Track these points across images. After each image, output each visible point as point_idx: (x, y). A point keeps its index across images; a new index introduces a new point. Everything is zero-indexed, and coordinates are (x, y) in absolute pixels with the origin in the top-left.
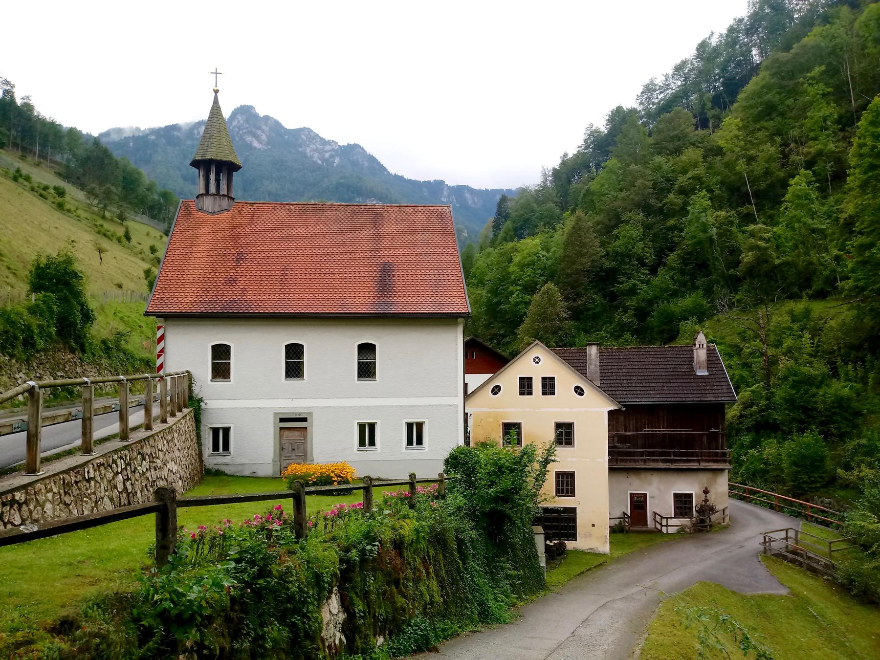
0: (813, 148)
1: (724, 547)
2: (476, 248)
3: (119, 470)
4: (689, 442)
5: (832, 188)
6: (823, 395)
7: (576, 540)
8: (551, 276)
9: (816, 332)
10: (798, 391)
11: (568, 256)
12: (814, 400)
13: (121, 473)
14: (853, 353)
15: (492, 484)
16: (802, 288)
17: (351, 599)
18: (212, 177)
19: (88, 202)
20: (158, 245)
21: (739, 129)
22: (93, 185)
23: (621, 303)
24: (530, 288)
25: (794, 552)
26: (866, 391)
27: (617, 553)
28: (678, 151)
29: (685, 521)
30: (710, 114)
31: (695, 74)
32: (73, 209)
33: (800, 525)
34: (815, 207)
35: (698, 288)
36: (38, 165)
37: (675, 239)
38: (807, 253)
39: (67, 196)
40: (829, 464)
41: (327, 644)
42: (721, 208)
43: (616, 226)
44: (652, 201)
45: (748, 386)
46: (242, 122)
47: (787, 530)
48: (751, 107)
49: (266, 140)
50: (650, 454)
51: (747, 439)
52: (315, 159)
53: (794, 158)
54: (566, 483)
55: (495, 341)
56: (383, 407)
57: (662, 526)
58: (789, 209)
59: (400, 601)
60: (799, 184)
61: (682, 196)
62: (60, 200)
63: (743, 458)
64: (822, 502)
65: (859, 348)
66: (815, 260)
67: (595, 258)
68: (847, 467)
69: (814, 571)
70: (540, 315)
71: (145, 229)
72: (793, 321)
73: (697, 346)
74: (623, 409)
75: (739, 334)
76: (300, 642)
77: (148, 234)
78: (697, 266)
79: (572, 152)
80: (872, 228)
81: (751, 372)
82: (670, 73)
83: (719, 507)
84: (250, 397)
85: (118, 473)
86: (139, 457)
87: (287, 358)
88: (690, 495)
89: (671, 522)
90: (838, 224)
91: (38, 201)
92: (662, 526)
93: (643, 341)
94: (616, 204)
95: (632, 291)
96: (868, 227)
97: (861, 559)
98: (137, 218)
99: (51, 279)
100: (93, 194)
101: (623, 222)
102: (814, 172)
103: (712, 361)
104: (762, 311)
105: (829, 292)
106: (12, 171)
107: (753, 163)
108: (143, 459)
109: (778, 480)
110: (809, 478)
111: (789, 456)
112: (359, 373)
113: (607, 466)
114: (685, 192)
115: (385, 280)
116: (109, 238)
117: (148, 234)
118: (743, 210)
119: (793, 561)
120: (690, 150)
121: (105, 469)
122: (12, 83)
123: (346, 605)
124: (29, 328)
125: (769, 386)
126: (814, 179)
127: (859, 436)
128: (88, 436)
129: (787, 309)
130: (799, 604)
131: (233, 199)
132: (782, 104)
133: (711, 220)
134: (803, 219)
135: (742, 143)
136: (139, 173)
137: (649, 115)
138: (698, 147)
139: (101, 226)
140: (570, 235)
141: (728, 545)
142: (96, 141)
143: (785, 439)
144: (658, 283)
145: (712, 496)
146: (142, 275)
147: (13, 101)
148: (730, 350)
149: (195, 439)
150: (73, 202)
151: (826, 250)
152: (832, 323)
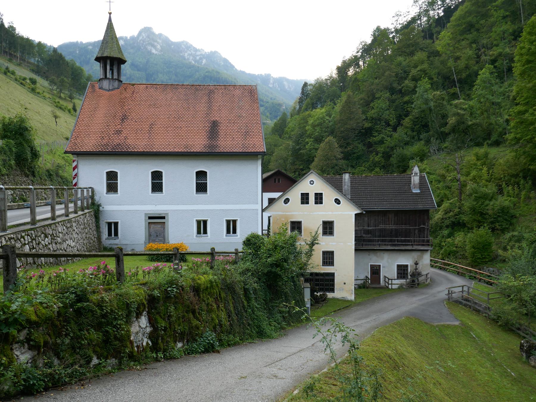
0: (495, 52)
1: (424, 297)
2: (289, 115)
3: (27, 242)
4: (407, 233)
5: (507, 77)
6: (492, 205)
7: (334, 292)
8: (332, 133)
9: (491, 166)
10: (478, 203)
11: (343, 120)
12: (487, 208)
13: (28, 244)
14: (513, 180)
15: (270, 256)
16: (485, 139)
17: (156, 319)
18: (108, 67)
19: (50, 87)
21: (451, 39)
22: (54, 77)
24: (319, 140)
25: (467, 300)
26: (519, 203)
27: (359, 300)
28: (412, 54)
29: (403, 281)
30: (434, 31)
31: (426, 5)
32: (41, 92)
33: (473, 284)
34: (495, 88)
35: (421, 140)
36: (19, 65)
37: (409, 109)
38: (488, 118)
39: (37, 84)
40: (494, 247)
41: (135, 345)
42: (437, 89)
43: (372, 101)
44: (395, 85)
45: (448, 200)
46: (145, 37)
47: (463, 287)
48: (458, 25)
50: (383, 241)
51: (446, 232)
52: (190, 61)
53: (483, 58)
54: (328, 258)
55: (297, 173)
58: (478, 90)
59: (195, 322)
60: (485, 73)
61: (414, 82)
63: (443, 244)
64: (489, 270)
65: (516, 176)
66: (493, 122)
67: (359, 121)
68: (505, 249)
69: (478, 311)
70: (324, 157)
72: (478, 160)
73: (414, 174)
74: (364, 212)
75: (445, 168)
76: (110, 342)
78: (422, 126)
80: (527, 100)
81: (450, 191)
83: (424, 273)
84: (130, 204)
85: (25, 244)
86: (42, 235)
87: (152, 180)
88: (407, 266)
89: (394, 282)
90: (509, 100)
91: (19, 87)
93: (387, 172)
94: (373, 87)
95: (381, 142)
96: (524, 100)
97: (505, 304)
100: (54, 83)
101: (376, 98)
102: (495, 67)
103: (422, 184)
106: (3, 69)
107: (458, 61)
108: (46, 236)
109: (464, 257)
110: (482, 255)
111: (470, 242)
114: (415, 79)
115: (214, 129)
116: (63, 110)
118: (452, 91)
119: (465, 305)
120: (419, 53)
121: (15, 241)
123: (152, 322)
125: (461, 200)
126: (494, 70)
127: (513, 231)
128: (4, 221)
129: (474, 152)
130: (465, 330)
131: (122, 81)
132: (478, 23)
133: (431, 97)
134: (486, 96)
135: (451, 48)
136: (82, 70)
138: (424, 51)
139: (59, 102)
140: (343, 107)
141: (427, 296)
142: (55, 50)
143: (468, 232)
144: (397, 137)
145: (420, 267)
148: (439, 178)
149: (94, 228)
150: (41, 88)
151: (501, 115)
152: (501, 161)
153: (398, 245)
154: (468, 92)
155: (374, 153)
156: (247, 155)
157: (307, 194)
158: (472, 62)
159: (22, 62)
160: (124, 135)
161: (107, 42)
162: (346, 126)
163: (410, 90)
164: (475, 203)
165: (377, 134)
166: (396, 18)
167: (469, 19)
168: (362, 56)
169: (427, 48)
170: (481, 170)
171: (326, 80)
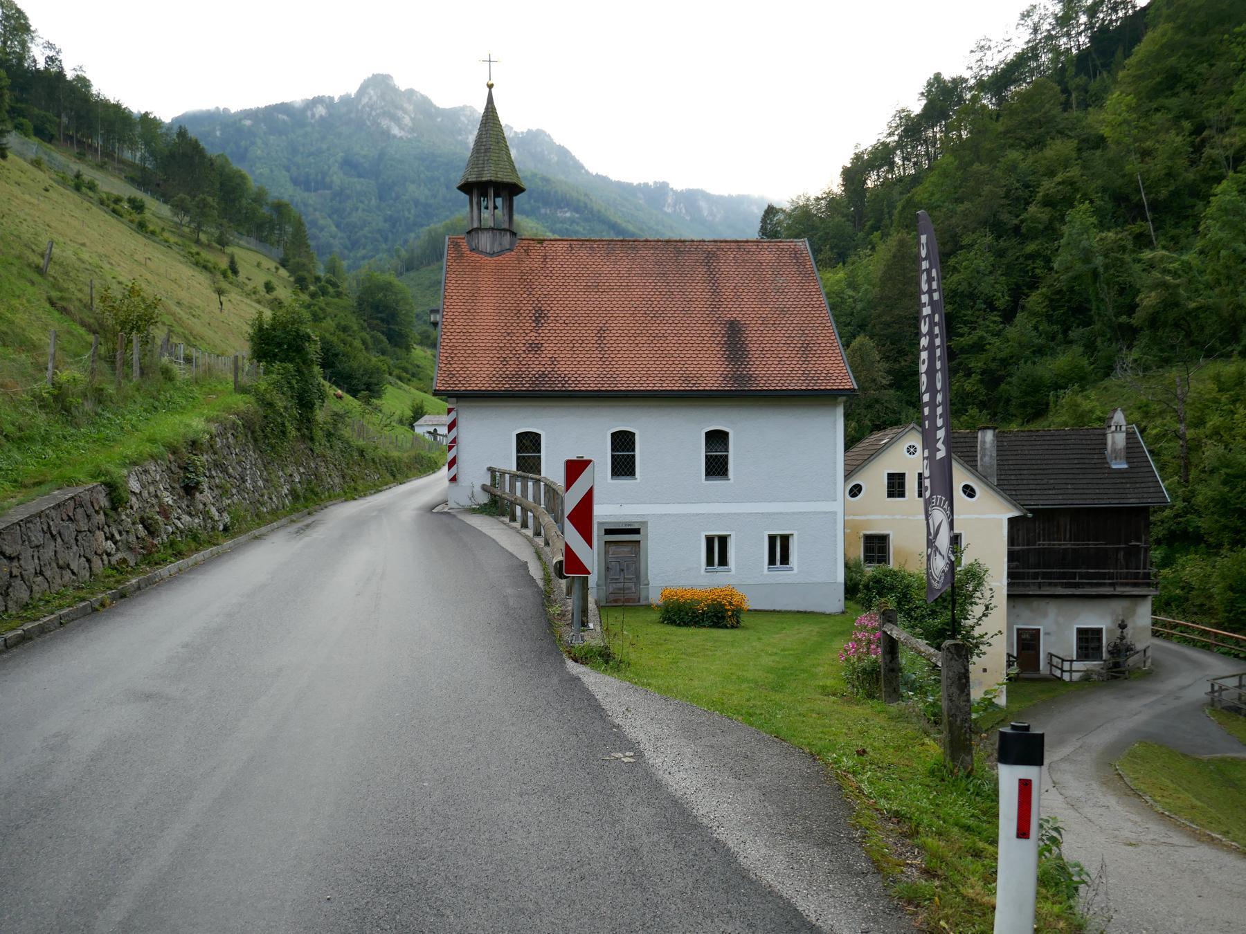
1: (1153, 698)
10: (1232, 489)
18: (475, 200)
19: (176, 219)
20: (275, 282)
22: (182, 195)
23: (960, 364)
27: (1015, 707)
28: (1038, 143)
32: (158, 230)
36: (101, 167)
37: (1038, 271)
44: (1004, 217)
46: (375, 98)
49: (410, 124)
50: (1045, 576)
56: (739, 514)
57: (1063, 671)
61: (1048, 209)
71: (255, 257)
73: (1113, 428)
74: (1030, 515)
77: (259, 265)
78: (1071, 310)
83: (1139, 646)
88: (1099, 631)
91: (112, 220)
92: (1063, 671)
94: (954, 221)
98: (241, 242)
99: (280, 345)
101: (962, 247)
103: (1132, 448)
104: (1173, 373)
113: (1005, 592)
115: (734, 340)
117: (259, 265)
118: (1136, 228)
122: (58, 47)
136: (243, 177)
139: (198, 254)
141: (1159, 696)
145: (1129, 632)
147: (61, 74)
150: (155, 220)
154: (1173, 232)
155: (961, 374)
157: (901, 476)
158: (1182, 162)
159: (108, 160)
160: (547, 352)
161: (487, 151)
163: (1041, 227)
164: (1227, 489)
165: (966, 329)
166: (979, 55)
167: (1172, 61)
168: (900, 145)
169: (1070, 130)
170: (1233, 412)
171: (817, 199)
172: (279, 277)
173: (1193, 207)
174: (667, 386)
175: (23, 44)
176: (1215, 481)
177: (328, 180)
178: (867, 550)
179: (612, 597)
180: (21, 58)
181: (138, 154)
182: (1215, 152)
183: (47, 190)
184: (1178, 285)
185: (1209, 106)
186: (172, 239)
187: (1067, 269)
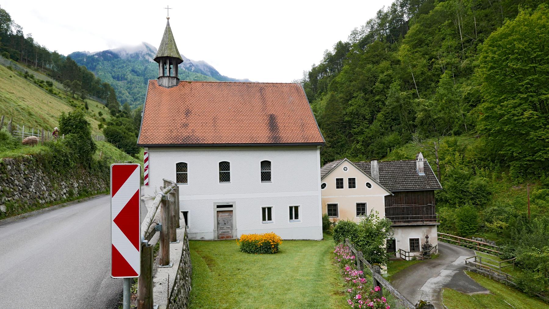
6: (472, 184)
18: (161, 65)
20: (102, 112)
23: (354, 139)
28: (377, 63)
29: (416, 254)
32: (57, 93)
37: (380, 106)
43: (350, 99)
50: (396, 218)
57: (406, 256)
61: (382, 85)
62: (50, 88)
71: (95, 103)
78: (393, 120)
79: (317, 64)
82: (365, 25)
83: (433, 245)
88: (418, 239)
92: (406, 256)
95: (361, 133)
101: (353, 97)
103: (426, 169)
104: (430, 141)
105: (461, 132)
106: (23, 73)
112: (220, 179)
117: (97, 106)
118: (411, 92)
124: (66, 156)
127: (491, 205)
137: (354, 45)
145: (429, 239)
146: (97, 127)
147: (22, 37)
150: (56, 89)
153: (411, 221)
155: (355, 142)
156: (307, 146)
158: (426, 69)
159: (40, 67)
162: (331, 120)
168: (328, 65)
172: (105, 111)
173: (431, 84)
174: (244, 142)
175: (8, 26)
176: (451, 180)
177: (126, 77)
178: (329, 210)
179: (220, 236)
180: (7, 30)
181: (52, 66)
182: (437, 66)
183: (11, 77)
184: (430, 110)
185: (433, 51)
186: (63, 96)
187: (390, 105)
